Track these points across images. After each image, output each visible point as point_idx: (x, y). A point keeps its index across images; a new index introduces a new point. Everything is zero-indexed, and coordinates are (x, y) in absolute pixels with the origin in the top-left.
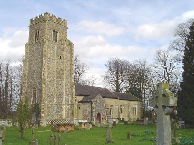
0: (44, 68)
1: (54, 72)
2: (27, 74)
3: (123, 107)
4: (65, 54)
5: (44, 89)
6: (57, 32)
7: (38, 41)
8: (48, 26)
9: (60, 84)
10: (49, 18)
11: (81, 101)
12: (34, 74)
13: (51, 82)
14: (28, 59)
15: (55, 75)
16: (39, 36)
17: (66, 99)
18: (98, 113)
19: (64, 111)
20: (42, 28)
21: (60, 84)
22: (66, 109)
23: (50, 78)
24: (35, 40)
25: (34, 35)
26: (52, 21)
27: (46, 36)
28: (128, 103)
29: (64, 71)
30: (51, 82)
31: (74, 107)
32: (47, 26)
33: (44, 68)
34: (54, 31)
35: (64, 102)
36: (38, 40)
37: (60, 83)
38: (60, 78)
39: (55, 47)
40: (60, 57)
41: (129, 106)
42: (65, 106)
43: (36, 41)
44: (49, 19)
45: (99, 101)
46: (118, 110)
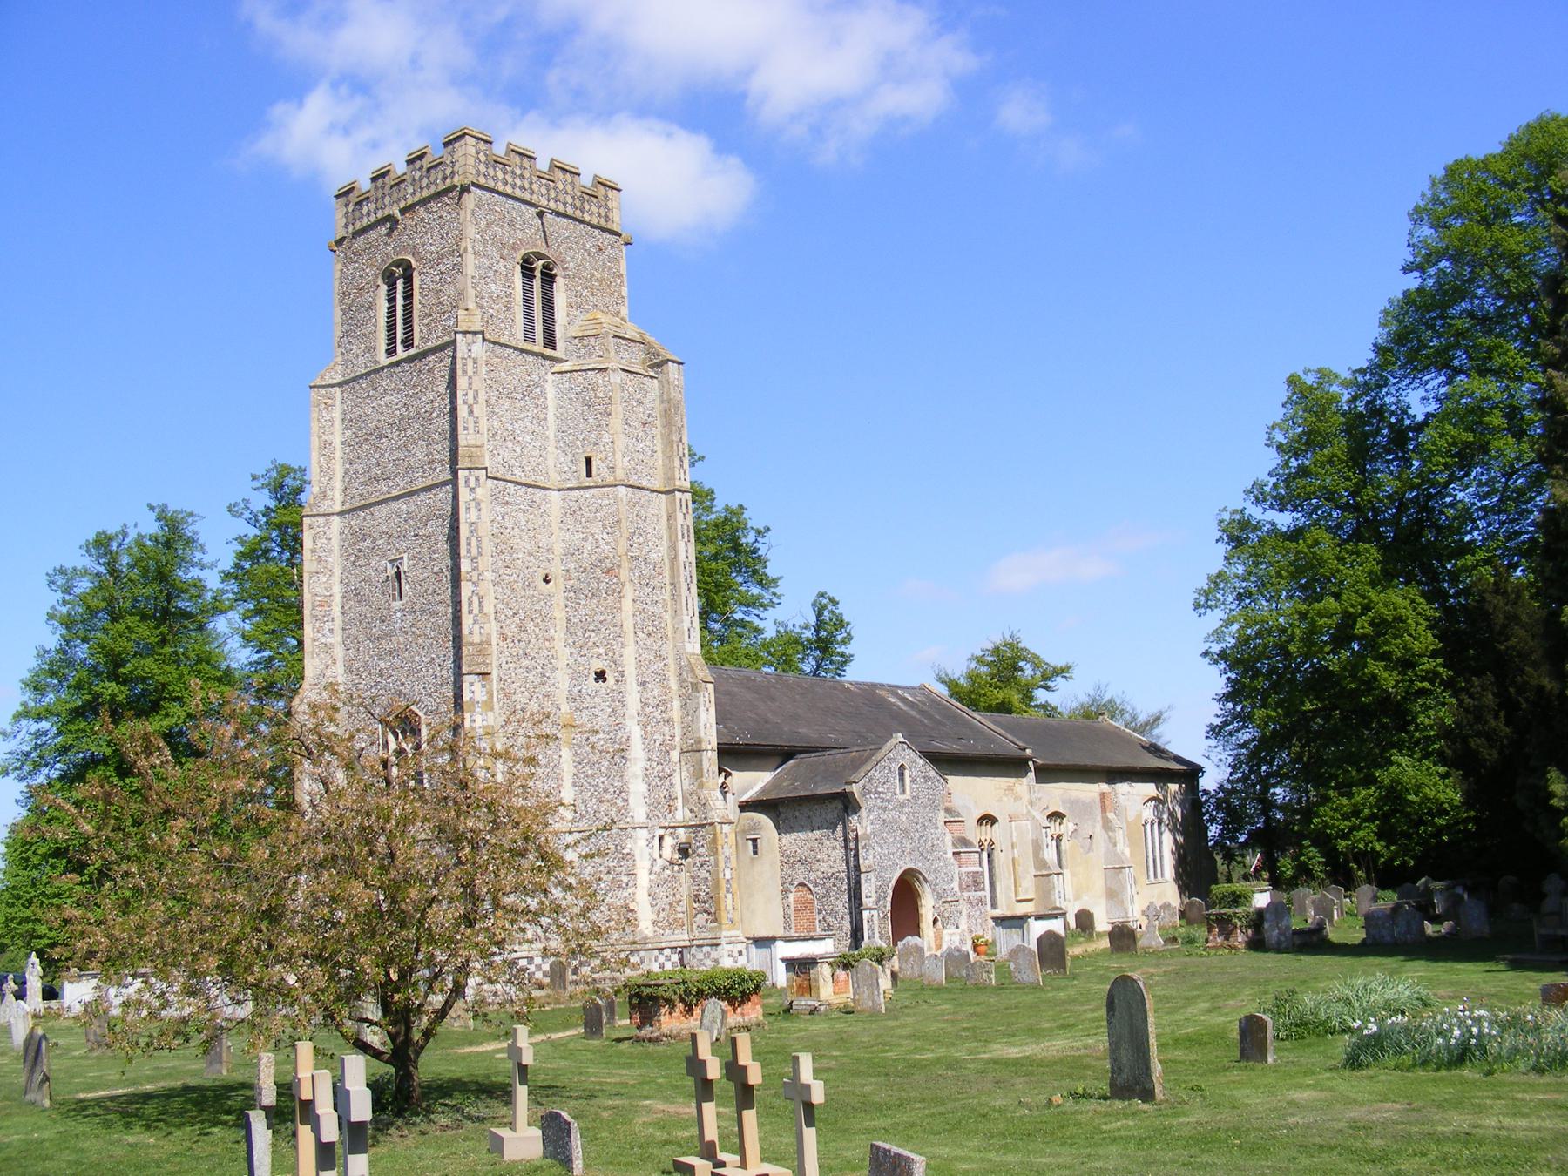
0: (474, 552)
1: (546, 580)
2: (336, 609)
3: (1071, 827)
4: (621, 441)
5: (478, 719)
6: (548, 278)
7: (412, 352)
8: (482, 233)
9: (601, 676)
10: (482, 168)
11: (763, 791)
12: (396, 604)
13: (525, 662)
14: (338, 497)
15: (559, 599)
16: (416, 314)
17: (651, 788)
18: (897, 875)
19: (644, 879)
20: (431, 244)
21: (601, 676)
22: (660, 862)
23: (522, 629)
24: (382, 345)
25: (371, 306)
26: (509, 190)
27: (472, 306)
28: (1103, 795)
29: (624, 574)
30: (525, 662)
31: (714, 840)
32: (471, 231)
33: (474, 552)
34: (527, 270)
35: (639, 812)
36: (408, 343)
37: (598, 665)
38: (596, 630)
39: (543, 392)
40: (589, 461)
41: (1110, 815)
42: (649, 842)
43: (391, 351)
44: (482, 181)
45: (903, 792)
46: (1037, 847)
